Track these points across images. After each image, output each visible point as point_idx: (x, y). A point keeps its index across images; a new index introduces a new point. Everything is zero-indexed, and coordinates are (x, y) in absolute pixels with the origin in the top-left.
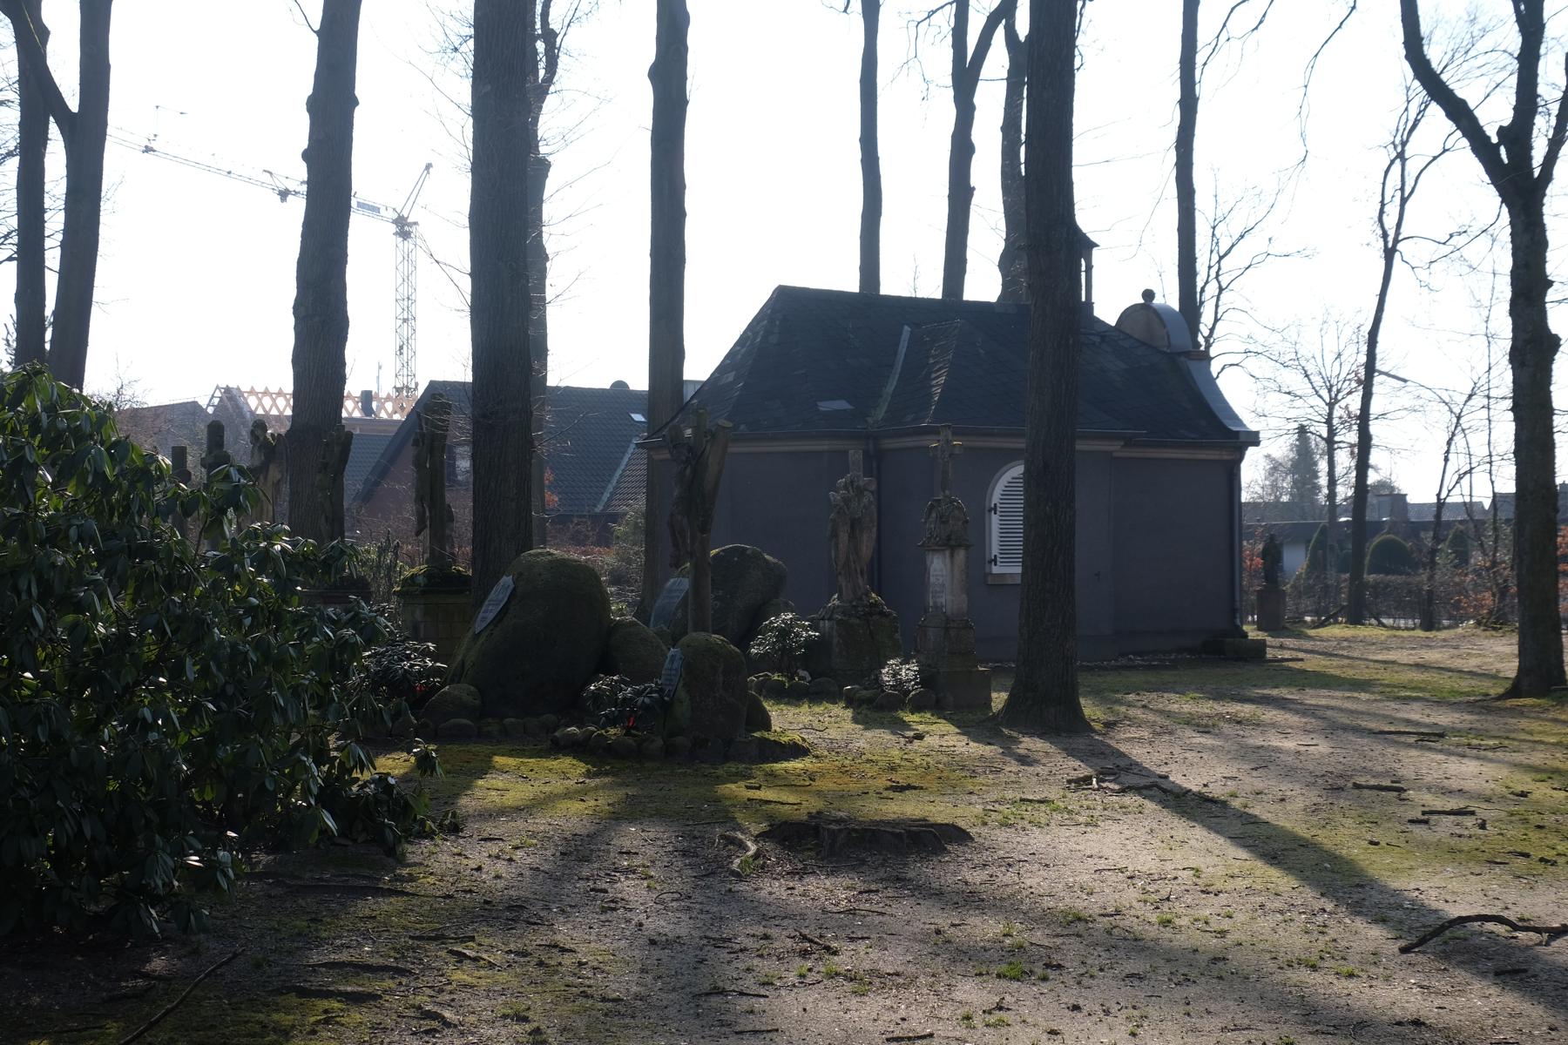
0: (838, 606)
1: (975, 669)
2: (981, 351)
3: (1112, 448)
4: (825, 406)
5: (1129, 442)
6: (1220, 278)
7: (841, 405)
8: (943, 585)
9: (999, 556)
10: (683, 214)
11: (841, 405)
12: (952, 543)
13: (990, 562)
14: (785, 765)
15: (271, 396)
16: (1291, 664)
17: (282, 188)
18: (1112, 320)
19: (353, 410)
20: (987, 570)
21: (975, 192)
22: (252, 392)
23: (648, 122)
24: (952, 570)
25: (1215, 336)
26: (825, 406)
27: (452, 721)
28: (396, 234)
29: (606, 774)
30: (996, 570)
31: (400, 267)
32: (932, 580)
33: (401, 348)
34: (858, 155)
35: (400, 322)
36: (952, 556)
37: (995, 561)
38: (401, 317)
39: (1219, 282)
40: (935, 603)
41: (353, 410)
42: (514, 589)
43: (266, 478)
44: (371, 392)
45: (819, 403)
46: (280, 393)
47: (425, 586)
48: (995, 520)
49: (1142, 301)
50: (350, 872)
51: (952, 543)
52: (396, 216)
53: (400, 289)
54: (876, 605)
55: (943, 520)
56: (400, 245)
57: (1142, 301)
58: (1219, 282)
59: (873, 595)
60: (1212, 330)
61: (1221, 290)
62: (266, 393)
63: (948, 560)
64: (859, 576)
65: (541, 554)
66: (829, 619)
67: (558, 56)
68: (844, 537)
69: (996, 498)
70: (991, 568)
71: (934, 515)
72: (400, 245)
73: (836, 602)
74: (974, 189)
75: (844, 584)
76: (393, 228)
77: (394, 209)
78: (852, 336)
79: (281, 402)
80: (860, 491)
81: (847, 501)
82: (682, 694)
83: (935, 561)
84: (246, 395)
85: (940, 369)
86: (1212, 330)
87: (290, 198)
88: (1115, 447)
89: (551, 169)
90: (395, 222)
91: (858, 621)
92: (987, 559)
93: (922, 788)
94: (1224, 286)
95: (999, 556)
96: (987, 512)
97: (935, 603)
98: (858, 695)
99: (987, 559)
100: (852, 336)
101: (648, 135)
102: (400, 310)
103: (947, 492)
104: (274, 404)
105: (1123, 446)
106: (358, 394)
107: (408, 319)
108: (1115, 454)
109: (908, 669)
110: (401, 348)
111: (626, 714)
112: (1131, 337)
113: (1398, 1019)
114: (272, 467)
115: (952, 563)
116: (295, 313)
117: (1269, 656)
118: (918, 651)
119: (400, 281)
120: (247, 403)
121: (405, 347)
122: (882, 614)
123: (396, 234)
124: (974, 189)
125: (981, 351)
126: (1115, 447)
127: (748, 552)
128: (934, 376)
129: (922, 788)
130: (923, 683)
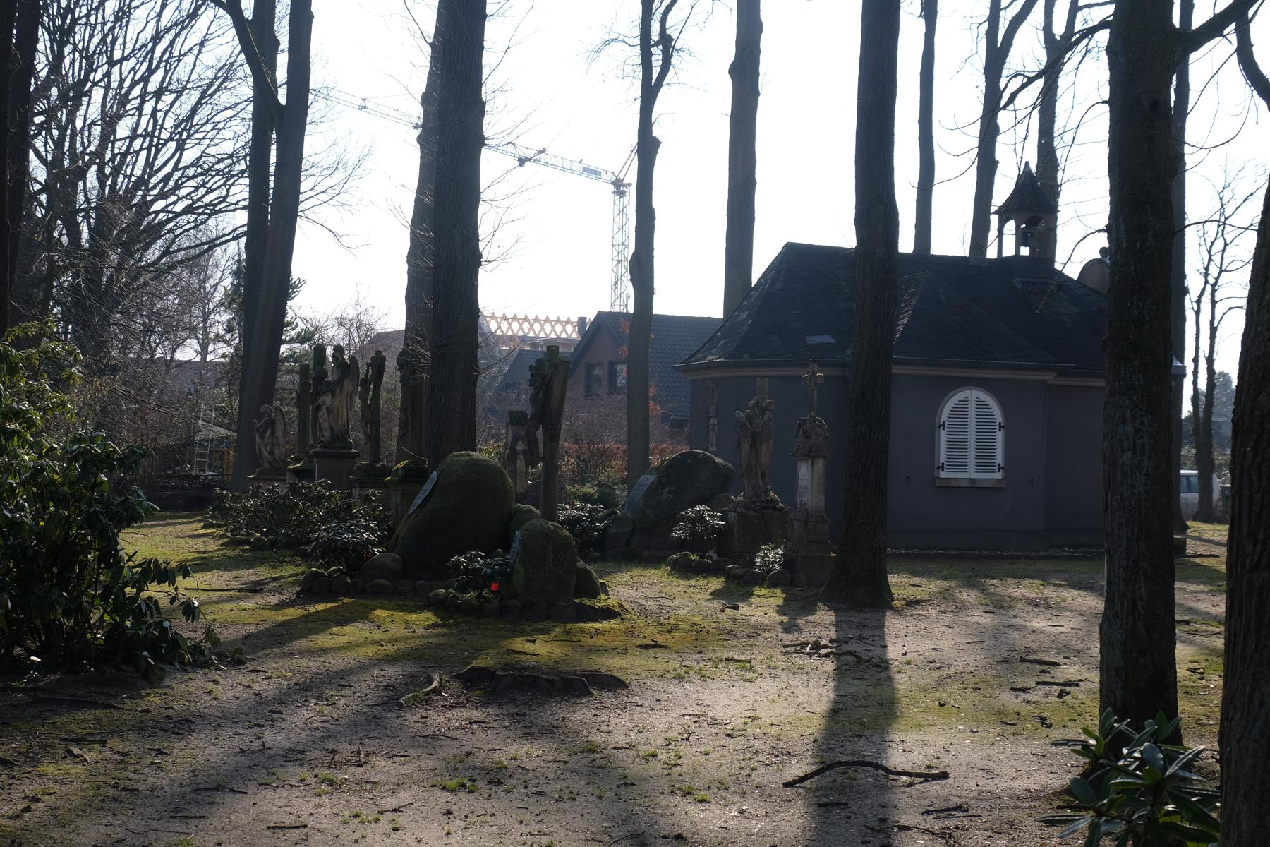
0: (742, 502)
1: (827, 555)
2: (943, 298)
3: (1047, 378)
4: (813, 340)
5: (1062, 373)
6: (1225, 236)
7: (827, 339)
8: (806, 488)
9: (946, 463)
10: (754, 183)
11: (827, 339)
12: (812, 454)
13: (938, 469)
14: (582, 625)
15: (540, 323)
16: (1198, 561)
17: (522, 155)
18: (1073, 272)
19: (572, 334)
20: (936, 475)
21: (999, 165)
22: (493, 317)
23: (728, 110)
24: (812, 476)
25: (1219, 284)
26: (813, 340)
27: (376, 581)
28: (613, 193)
29: (448, 626)
30: (943, 475)
31: (617, 219)
32: (800, 482)
33: (616, 283)
34: (917, 133)
35: (615, 263)
36: (812, 465)
37: (942, 467)
38: (617, 259)
39: (1225, 240)
40: (801, 501)
41: (572, 334)
42: (437, 482)
43: (341, 390)
44: (585, 318)
45: (808, 338)
46: (568, 322)
47: (402, 477)
48: (943, 434)
49: (1100, 257)
50: (105, 691)
51: (812, 454)
52: (614, 178)
53: (616, 237)
54: (772, 501)
55: (807, 436)
56: (617, 202)
57: (1100, 257)
58: (1225, 240)
59: (771, 493)
60: (1217, 279)
61: (1226, 245)
62: (515, 318)
63: (810, 467)
64: (760, 479)
65: (462, 455)
66: (734, 512)
67: (672, 56)
68: (746, 447)
69: (944, 416)
70: (939, 473)
71: (801, 431)
72: (617, 202)
73: (741, 498)
74: (998, 162)
75: (746, 483)
76: (612, 188)
77: (613, 173)
78: (843, 284)
79: (569, 328)
80: (763, 410)
81: (750, 419)
82: (519, 567)
83: (802, 467)
84: (488, 319)
85: (906, 312)
86: (1217, 279)
87: (527, 164)
88: (1049, 377)
89: (661, 146)
90: (613, 183)
91: (755, 514)
92: (936, 466)
93: (666, 647)
94: (1228, 242)
95: (946, 463)
96: (937, 428)
97: (801, 501)
98: (733, 573)
99: (936, 466)
100: (843, 284)
101: (728, 119)
102: (615, 253)
103: (813, 413)
104: (553, 330)
105: (1056, 377)
106: (576, 320)
107: (621, 261)
108: (1050, 382)
109: (777, 553)
110: (616, 283)
111: (477, 580)
112: (1086, 286)
113: (678, 830)
114: (346, 381)
115: (812, 470)
116: (408, 262)
117: (1189, 551)
118: (788, 539)
119: (616, 230)
120: (489, 326)
121: (619, 282)
122: (775, 509)
123: (613, 193)
124: (998, 162)
125: (943, 298)
126: (1049, 377)
127: (700, 456)
128: (901, 316)
129: (666, 647)
130: (784, 566)
